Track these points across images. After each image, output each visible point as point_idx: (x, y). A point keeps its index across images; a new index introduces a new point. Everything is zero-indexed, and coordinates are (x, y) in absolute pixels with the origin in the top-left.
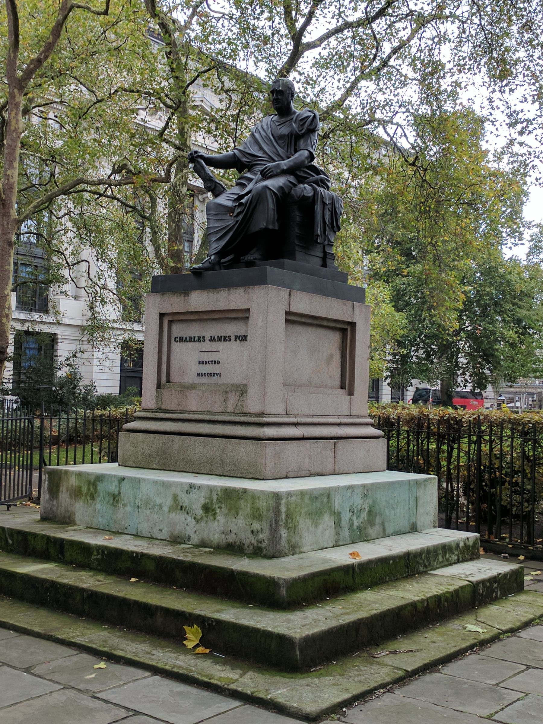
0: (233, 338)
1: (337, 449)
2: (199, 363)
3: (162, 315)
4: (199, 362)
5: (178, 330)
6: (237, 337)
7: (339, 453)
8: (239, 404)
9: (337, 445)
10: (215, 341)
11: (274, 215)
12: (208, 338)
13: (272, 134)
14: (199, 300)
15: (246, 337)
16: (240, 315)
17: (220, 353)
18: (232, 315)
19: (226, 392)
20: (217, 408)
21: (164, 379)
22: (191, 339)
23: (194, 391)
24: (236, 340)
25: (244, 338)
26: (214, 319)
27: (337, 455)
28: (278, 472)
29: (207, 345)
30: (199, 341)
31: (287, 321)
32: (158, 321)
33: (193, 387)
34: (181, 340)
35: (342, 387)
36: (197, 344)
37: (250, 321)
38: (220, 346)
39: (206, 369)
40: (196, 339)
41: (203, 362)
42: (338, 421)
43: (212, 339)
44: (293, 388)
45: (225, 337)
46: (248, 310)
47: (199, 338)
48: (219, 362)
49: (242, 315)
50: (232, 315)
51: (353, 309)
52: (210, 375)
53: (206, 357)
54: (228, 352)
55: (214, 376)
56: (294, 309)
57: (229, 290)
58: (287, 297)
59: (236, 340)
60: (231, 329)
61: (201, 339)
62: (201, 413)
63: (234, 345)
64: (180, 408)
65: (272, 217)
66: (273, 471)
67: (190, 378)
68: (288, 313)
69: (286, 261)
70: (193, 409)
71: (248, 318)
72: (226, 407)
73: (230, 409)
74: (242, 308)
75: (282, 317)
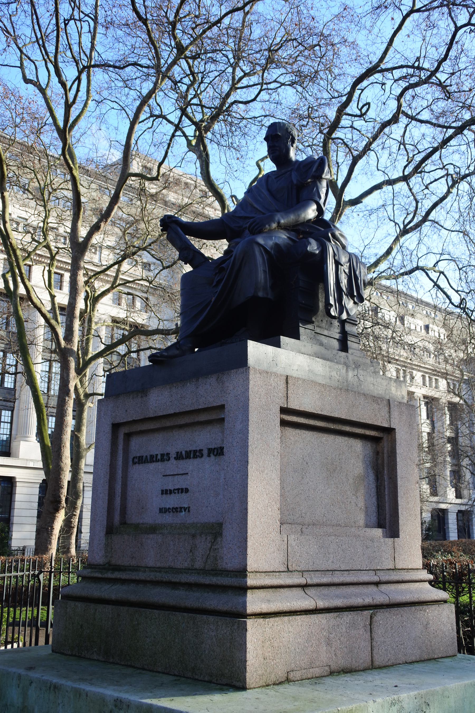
0: (205, 452)
1: (375, 625)
2: (162, 494)
3: (116, 427)
4: (162, 491)
5: (139, 446)
6: (211, 451)
7: (379, 631)
8: (212, 554)
9: (375, 619)
10: (183, 459)
11: (265, 278)
12: (173, 455)
13: (269, 190)
14: (161, 400)
15: (222, 448)
16: (213, 416)
17: (188, 477)
18: (203, 417)
19: (194, 536)
20: (182, 562)
21: (117, 518)
22: (152, 459)
23: (151, 536)
24: (209, 456)
25: (218, 452)
26: (181, 427)
27: (375, 635)
28: (270, 673)
29: (172, 466)
30: (162, 460)
31: (284, 423)
32: (109, 436)
33: (153, 529)
34: (141, 460)
35: (380, 525)
36: (159, 465)
37: (226, 423)
38: (190, 465)
39: (173, 501)
40: (159, 457)
41: (166, 490)
42: (376, 579)
43: (179, 457)
44: (299, 528)
45: (195, 451)
46: (222, 407)
47: (162, 455)
48: (187, 490)
49: (214, 416)
50: (203, 417)
51: (390, 409)
52: (176, 510)
53: (171, 484)
54: (199, 473)
55: (181, 511)
56: (294, 405)
57: (197, 380)
58: (376, 657)
59: (209, 456)
60: (203, 438)
61: (165, 457)
62: (159, 569)
63: (207, 463)
64: (134, 563)
65: (263, 281)
66: (260, 672)
67: (151, 517)
68: (284, 410)
69: (284, 339)
70: (151, 564)
71: (223, 420)
72: (193, 560)
73: (199, 564)
74: (215, 404)
75: (277, 417)
